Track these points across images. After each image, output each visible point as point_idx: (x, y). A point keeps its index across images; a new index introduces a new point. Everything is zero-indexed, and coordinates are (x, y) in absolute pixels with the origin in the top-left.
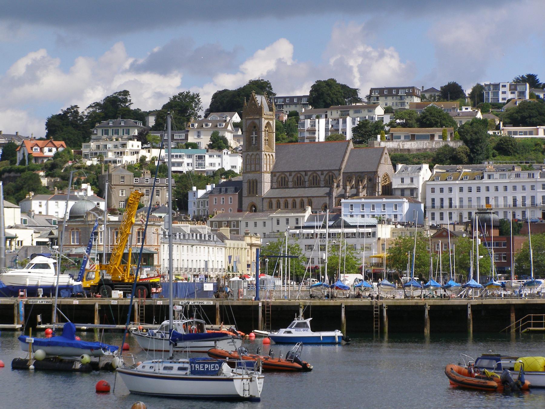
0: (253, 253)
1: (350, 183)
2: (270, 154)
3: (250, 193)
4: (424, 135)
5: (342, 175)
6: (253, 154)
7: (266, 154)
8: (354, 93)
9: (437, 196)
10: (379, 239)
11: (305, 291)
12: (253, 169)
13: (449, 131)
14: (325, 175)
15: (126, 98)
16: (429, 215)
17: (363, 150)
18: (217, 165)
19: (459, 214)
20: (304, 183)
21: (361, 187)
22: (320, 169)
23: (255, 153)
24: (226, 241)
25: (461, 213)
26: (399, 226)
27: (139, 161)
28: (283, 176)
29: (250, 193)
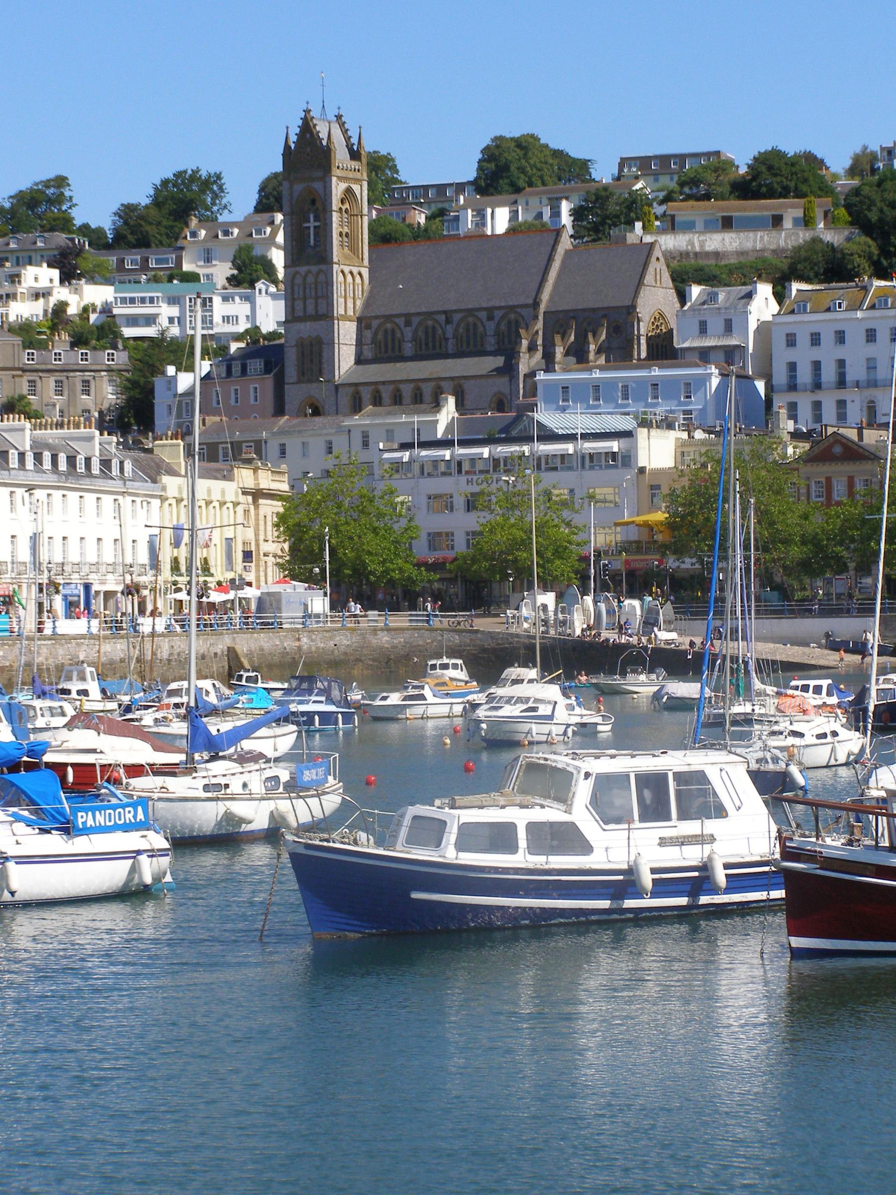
0: (261, 518)
1: (563, 339)
2: (355, 270)
3: (303, 374)
4: (755, 218)
5: (541, 317)
6: (309, 272)
7: (342, 272)
8: (581, 168)
9: (804, 356)
10: (642, 470)
11: (407, 629)
12: (311, 309)
13: (820, 206)
14: (497, 319)
15: (62, 194)
16: (780, 404)
17: (598, 252)
18: (242, 320)
19: (865, 405)
20: (443, 344)
21: (592, 347)
22: (484, 305)
23: (314, 269)
24: (166, 479)
25: (873, 402)
26: (699, 435)
27: (50, 315)
28: (389, 326)
29: (303, 374)
